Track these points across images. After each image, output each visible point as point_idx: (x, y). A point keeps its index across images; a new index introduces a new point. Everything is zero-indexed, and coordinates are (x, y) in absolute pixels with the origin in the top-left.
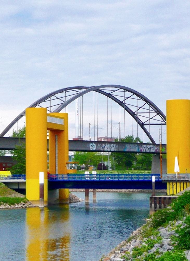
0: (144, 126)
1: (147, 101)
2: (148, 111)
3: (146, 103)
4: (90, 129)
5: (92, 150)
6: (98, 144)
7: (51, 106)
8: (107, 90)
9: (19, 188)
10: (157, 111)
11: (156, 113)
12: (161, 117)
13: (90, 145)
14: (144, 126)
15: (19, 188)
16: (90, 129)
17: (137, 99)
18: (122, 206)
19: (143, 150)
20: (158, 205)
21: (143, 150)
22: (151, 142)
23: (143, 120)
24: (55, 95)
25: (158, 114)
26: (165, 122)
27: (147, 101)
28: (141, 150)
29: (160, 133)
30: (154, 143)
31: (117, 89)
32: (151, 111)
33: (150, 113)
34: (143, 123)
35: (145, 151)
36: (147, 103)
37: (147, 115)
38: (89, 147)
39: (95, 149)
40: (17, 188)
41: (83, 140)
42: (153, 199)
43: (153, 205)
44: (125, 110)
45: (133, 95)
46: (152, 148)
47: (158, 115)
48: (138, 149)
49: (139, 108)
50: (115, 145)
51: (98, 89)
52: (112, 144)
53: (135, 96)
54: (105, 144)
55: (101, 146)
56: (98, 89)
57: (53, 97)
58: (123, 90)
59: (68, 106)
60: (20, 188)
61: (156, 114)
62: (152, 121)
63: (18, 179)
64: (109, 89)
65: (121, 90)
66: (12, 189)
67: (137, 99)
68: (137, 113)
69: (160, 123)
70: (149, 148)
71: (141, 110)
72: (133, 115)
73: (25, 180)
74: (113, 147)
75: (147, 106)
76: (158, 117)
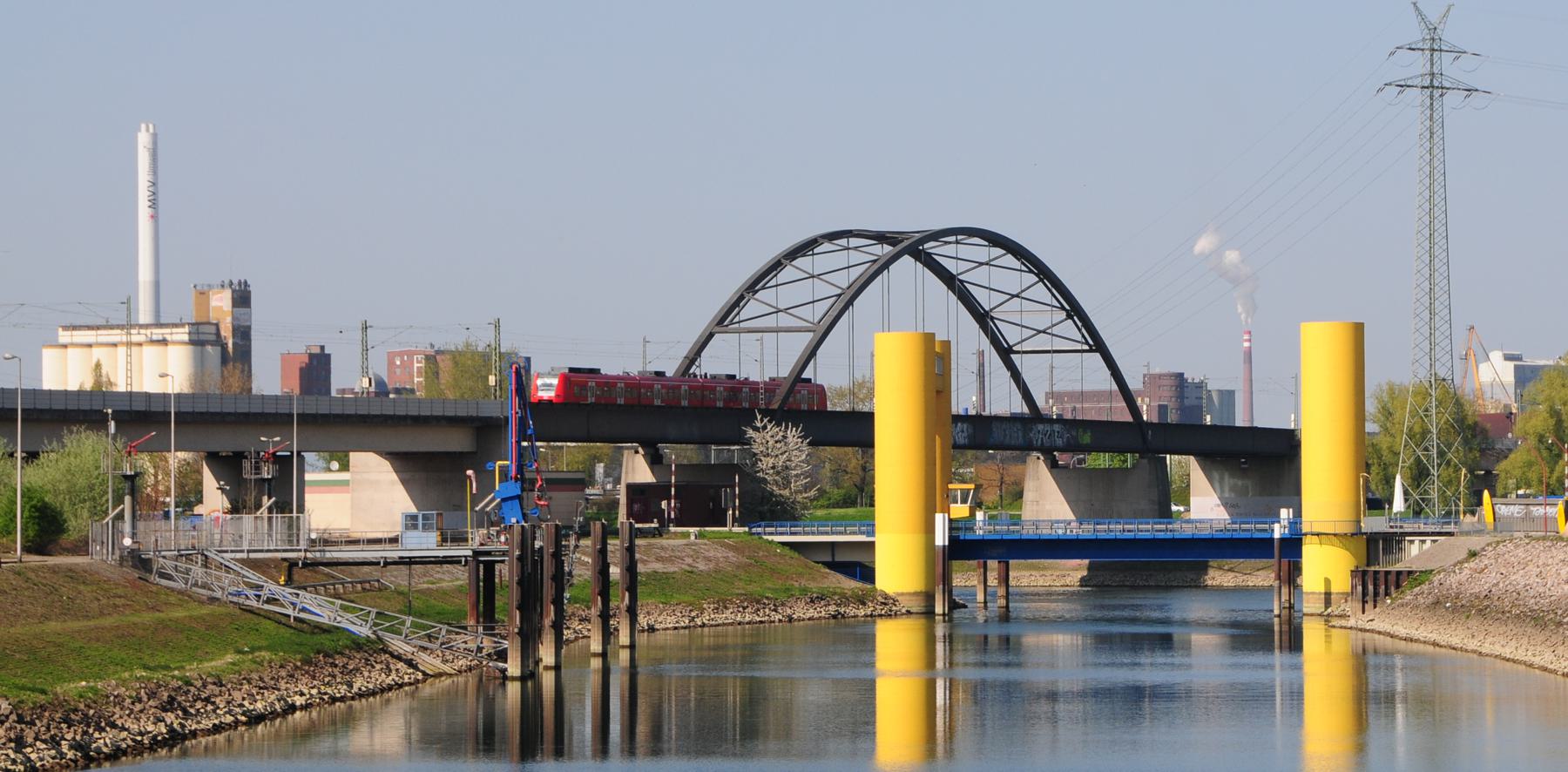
0: (1012, 355)
3: (1037, 279)
4: (644, 357)
7: (811, 305)
9: (833, 559)
10: (1068, 308)
11: (1065, 314)
14: (1013, 356)
15: (833, 559)
16: (644, 357)
20: (1371, 588)
23: (1011, 335)
24: (793, 263)
25: (1069, 316)
26: (1087, 343)
27: (1044, 273)
28: (1031, 441)
34: (1010, 347)
36: (1041, 280)
40: (829, 559)
41: (1237, 425)
42: (1360, 575)
43: (1360, 588)
44: (959, 302)
45: (1004, 255)
46: (1058, 432)
47: (1070, 321)
48: (1024, 437)
53: (1010, 260)
57: (787, 273)
59: (854, 303)
60: (837, 559)
61: (1063, 315)
63: (792, 534)
66: (818, 563)
70: (1050, 435)
72: (983, 318)
73: (872, 533)
75: (1041, 292)
76: (1070, 329)
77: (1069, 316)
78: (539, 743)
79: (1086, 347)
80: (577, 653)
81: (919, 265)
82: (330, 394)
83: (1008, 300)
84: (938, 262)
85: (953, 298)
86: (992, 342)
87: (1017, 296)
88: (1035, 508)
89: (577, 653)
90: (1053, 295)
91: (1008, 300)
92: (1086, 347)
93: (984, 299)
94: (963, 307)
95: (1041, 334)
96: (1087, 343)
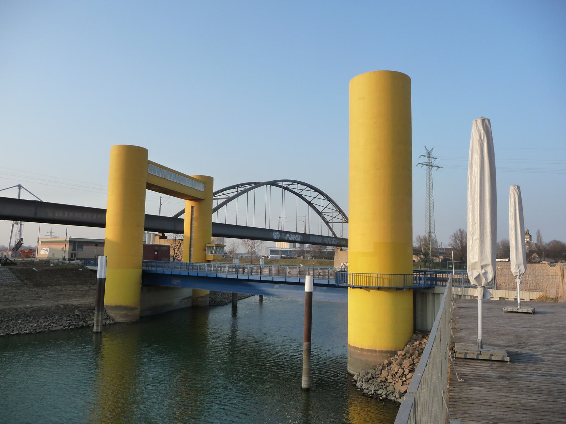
1: (316, 190)
2: (332, 211)
3: (319, 194)
4: (160, 203)
5: (275, 238)
6: (283, 234)
8: (285, 184)
12: (342, 216)
13: (274, 234)
16: (160, 203)
17: (310, 191)
18: (190, 377)
19: (326, 242)
21: (326, 242)
22: (333, 236)
23: (328, 218)
25: (340, 213)
26: (345, 220)
27: (331, 201)
29: (342, 231)
30: (336, 237)
31: (291, 183)
32: (334, 211)
33: (333, 212)
35: (328, 243)
36: (331, 203)
37: (331, 214)
38: (273, 235)
39: (278, 238)
49: (324, 208)
50: (299, 236)
51: (272, 183)
52: (297, 235)
53: (308, 189)
54: (290, 234)
55: (285, 236)
56: (272, 183)
58: (296, 184)
61: (338, 213)
62: (335, 220)
64: (282, 183)
65: (295, 184)
67: (310, 191)
68: (323, 212)
69: (341, 221)
71: (326, 210)
72: (320, 214)
74: (298, 237)
75: (331, 206)
76: (340, 216)
77: (340, 213)
78: (524, 300)
79: (345, 221)
80: (96, 313)
81: (309, 206)
82: (305, 290)
83: (305, 189)
84: (314, 206)
85: (321, 219)
86: (332, 229)
87: (334, 217)
88: (336, 260)
89: (96, 313)
90: (343, 217)
91: (305, 189)
92: (345, 221)
93: (308, 199)
94: (324, 222)
95: (303, 189)
96: (345, 220)
